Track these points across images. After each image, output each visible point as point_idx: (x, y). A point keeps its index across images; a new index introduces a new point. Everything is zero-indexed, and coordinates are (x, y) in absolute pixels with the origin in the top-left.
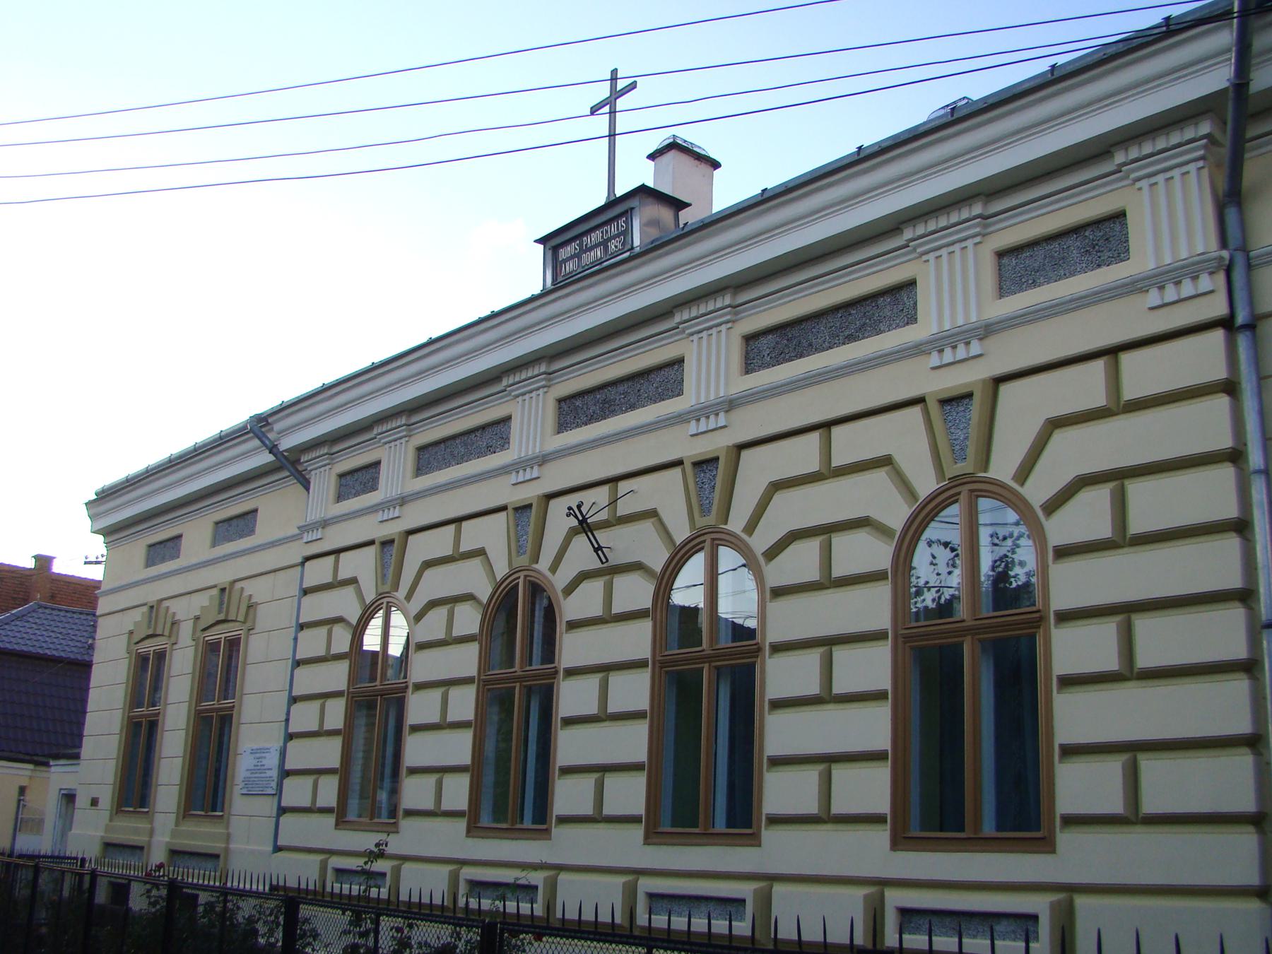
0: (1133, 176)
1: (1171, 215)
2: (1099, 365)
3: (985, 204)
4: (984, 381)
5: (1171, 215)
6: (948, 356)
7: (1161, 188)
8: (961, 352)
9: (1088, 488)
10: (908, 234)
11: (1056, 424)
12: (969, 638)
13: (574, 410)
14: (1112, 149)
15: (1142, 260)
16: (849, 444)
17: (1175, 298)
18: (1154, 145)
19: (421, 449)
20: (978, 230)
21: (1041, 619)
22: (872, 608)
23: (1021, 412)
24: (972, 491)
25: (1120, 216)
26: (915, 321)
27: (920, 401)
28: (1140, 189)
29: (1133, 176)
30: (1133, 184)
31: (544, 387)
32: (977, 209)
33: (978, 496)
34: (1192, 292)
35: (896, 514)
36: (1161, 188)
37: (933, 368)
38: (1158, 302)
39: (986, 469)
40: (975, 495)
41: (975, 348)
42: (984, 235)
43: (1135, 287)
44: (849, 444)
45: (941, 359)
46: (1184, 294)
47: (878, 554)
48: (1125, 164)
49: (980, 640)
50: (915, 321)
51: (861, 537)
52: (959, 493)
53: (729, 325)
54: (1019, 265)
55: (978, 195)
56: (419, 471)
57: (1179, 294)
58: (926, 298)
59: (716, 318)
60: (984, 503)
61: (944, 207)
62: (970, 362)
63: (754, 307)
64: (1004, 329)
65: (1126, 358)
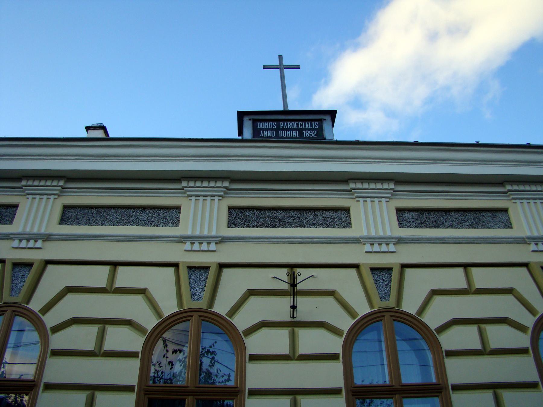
0: (356, 195)
1: (44, 212)
2: (107, 268)
3: (395, 185)
4: (41, 260)
5: (44, 212)
6: (24, 244)
7: (37, 200)
8: (204, 246)
9: (264, 328)
10: (352, 185)
11: (252, 293)
12: (191, 397)
13: (238, 216)
14: (349, 181)
15: (186, 228)
16: (126, 277)
17: (190, 249)
18: (39, 183)
19: (66, 208)
20: (57, 192)
21: (35, 386)
22: (128, 372)
23: (234, 284)
24: (14, 311)
25: (178, 208)
26: (400, 227)
27: (176, 265)
28: (28, 198)
29: (356, 195)
30: (188, 197)
31: (219, 196)
32: (226, 184)
33: (16, 315)
34: (206, 248)
35: (150, 322)
36: (37, 200)
37: (186, 251)
38: (16, 245)
39: (28, 303)
40: (16, 314)
41: (213, 246)
42: (59, 196)
43: (10, 237)
44: (126, 277)
45: (27, 244)
46: (194, 248)
47: (136, 343)
48: (186, 187)
49: (196, 399)
50: (400, 227)
51: (125, 330)
52: (6, 311)
53: (56, 197)
54: (238, 216)
55: (229, 178)
56: (63, 221)
57: (34, 245)
58: (21, 215)
59: (33, 190)
60: (19, 320)
61: (208, 178)
62: (34, 250)
63: (404, 195)
64: (231, 242)
65: (120, 269)
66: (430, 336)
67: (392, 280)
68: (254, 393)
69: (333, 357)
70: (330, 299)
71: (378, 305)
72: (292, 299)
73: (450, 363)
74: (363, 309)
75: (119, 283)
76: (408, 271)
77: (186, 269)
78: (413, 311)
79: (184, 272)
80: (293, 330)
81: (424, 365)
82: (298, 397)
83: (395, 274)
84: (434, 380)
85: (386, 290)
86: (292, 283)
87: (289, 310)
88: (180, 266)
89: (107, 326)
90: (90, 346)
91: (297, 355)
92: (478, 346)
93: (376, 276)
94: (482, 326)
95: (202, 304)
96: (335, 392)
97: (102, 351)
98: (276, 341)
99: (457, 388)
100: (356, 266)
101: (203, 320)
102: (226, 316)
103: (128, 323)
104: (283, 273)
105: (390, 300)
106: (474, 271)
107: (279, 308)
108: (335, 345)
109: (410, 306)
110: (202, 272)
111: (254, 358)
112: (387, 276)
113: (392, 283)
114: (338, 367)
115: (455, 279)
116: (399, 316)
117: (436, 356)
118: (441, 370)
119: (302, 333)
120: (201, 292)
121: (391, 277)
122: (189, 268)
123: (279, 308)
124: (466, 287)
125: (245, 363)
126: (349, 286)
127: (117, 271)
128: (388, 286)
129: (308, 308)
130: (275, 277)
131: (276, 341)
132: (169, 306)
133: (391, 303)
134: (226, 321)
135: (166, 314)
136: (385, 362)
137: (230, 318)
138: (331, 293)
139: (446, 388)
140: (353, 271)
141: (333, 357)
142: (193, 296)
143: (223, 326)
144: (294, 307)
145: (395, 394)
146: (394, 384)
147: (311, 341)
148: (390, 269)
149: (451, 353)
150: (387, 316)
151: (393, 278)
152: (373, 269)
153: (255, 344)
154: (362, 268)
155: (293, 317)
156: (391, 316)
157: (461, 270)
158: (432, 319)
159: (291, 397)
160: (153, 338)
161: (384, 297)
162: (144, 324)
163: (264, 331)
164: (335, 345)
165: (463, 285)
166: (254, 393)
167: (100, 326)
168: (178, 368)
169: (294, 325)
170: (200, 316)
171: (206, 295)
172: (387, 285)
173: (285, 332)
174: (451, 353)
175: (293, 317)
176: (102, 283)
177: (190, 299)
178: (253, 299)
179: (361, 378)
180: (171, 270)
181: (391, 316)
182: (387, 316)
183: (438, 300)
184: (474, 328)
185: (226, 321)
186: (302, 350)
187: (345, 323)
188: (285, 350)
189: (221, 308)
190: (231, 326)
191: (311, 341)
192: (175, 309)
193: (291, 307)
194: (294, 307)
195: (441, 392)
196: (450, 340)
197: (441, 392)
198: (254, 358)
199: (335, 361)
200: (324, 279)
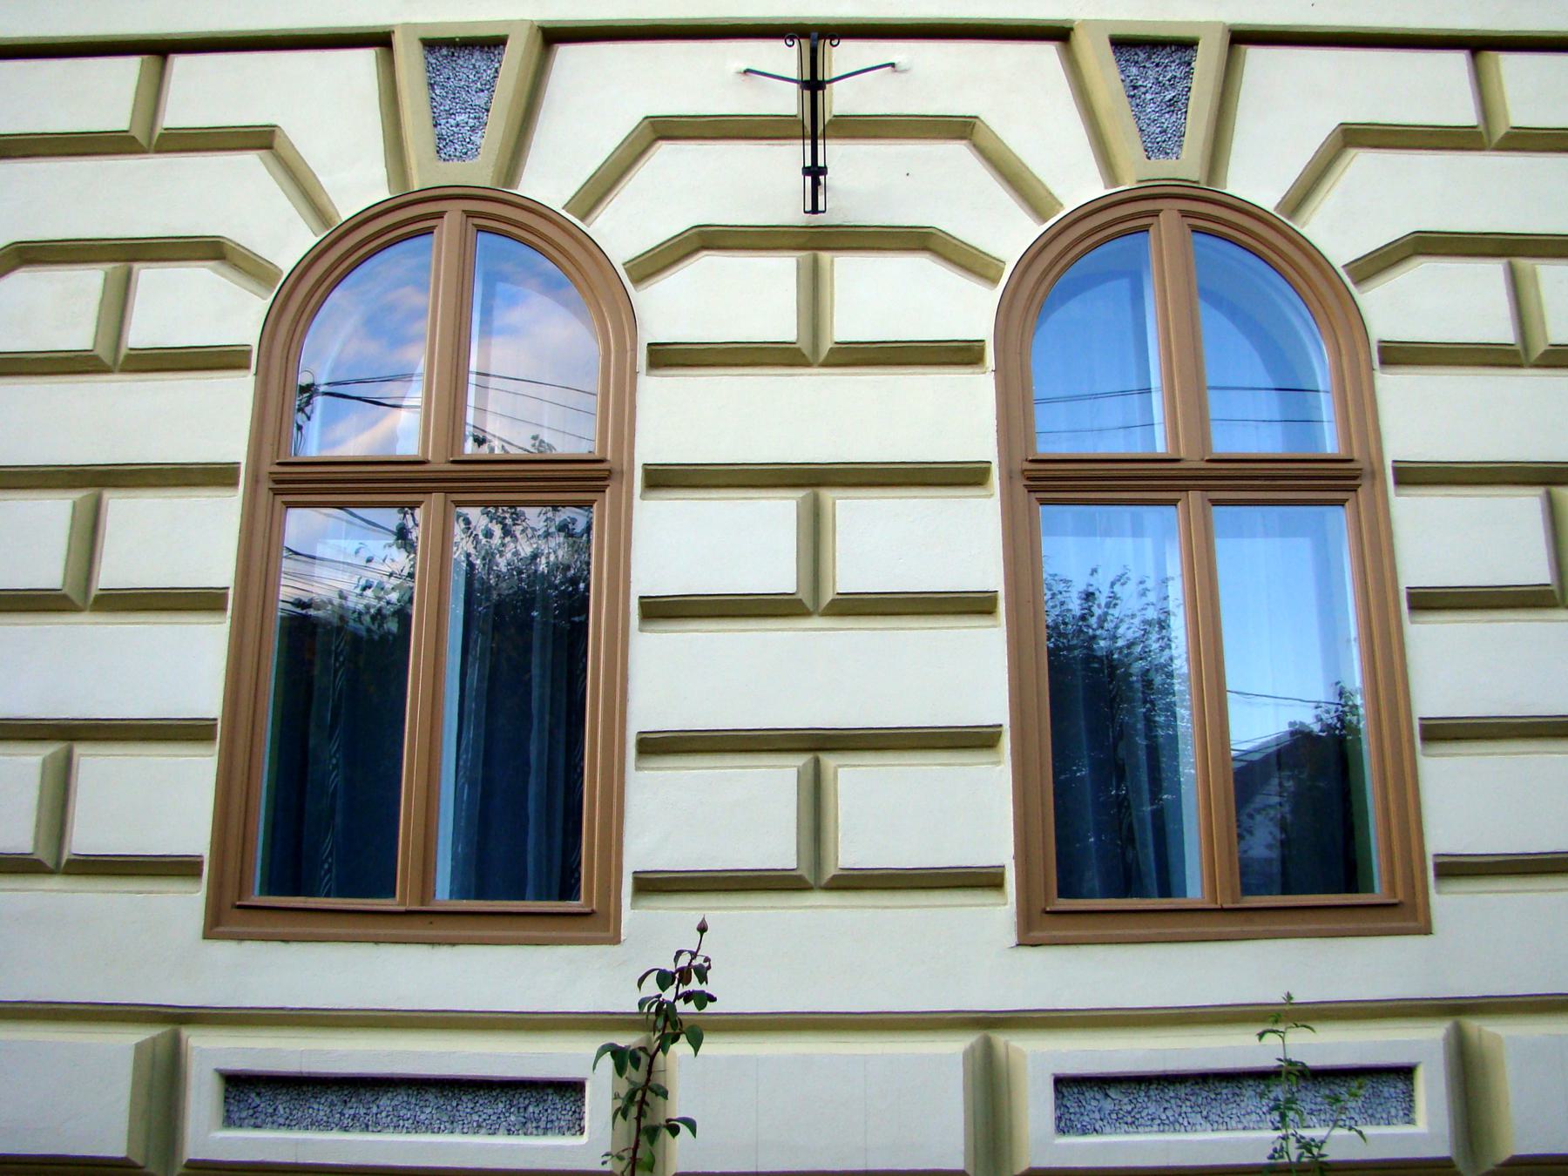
11: (664, 129)
23: (592, 102)
27: (380, 40)
35: (288, 241)
44: (201, 92)
47: (239, 316)
51: (200, 276)
66: (1325, 290)
67: (1194, 86)
68: (662, 479)
69: (963, 354)
70: (958, 151)
71: (1136, 170)
72: (808, 148)
73: (1397, 391)
74: (1078, 184)
75: (178, 114)
76: (1255, 57)
77: (417, 51)
78: (1267, 198)
79: (409, 58)
80: (816, 261)
81: (1293, 389)
82: (828, 495)
83: (1207, 61)
84: (1331, 445)
85: (1168, 120)
86: (807, 77)
87: (798, 183)
88: (397, 40)
89: (136, 266)
90: (80, 337)
91: (826, 346)
92: (1501, 331)
93: (1134, 70)
94: (1523, 263)
95: (478, 172)
96: (967, 476)
97: (124, 351)
98: (750, 297)
99: (1413, 476)
100: (1059, 34)
101: (481, 229)
102: (563, 213)
103: (211, 250)
104: (784, 57)
105: (1183, 156)
106: (1509, 64)
107: (764, 183)
108: (969, 310)
109: (1257, 179)
110: (477, 58)
111: (666, 357)
112: (1174, 70)
113: (1192, 94)
114: (975, 393)
115: (1436, 89)
116: (1216, 218)
117: (1345, 359)
118: (1361, 411)
119: (850, 274)
120: (473, 129)
121: (1188, 75)
122: (431, 45)
123: (764, 183)
124: (1473, 122)
125: (635, 374)
126: (1029, 104)
127: (167, 72)
128: (1175, 106)
129: (865, 180)
130: (747, 71)
131: (750, 297)
132: (357, 183)
133: (1187, 164)
134: (564, 230)
135: (346, 209)
136: (1155, 381)
137: (582, 219)
138: (960, 128)
139: (1375, 474)
140: (1048, 52)
141: (963, 354)
142: (443, 146)
143: (552, 244)
144: (815, 172)
145: (1186, 489)
146: (1182, 455)
147: (877, 296)
148: (1185, 46)
149: (1398, 355)
150: (1169, 212)
151: (1195, 76)
152: (1123, 45)
153: (673, 308)
154: (1081, 40)
155: (815, 210)
156: (1185, 214)
157: (1458, 60)
158: (1339, 229)
159: (800, 493)
160: (301, 296)
161: (1160, 144)
162: (264, 250)
163: (707, 262)
164: (969, 310)
165: (1464, 114)
166: (662, 479)
167: (109, 266)
168: (560, 553)
169: (817, 240)
170: (470, 214)
171: (493, 137)
172: (1172, 103)
173: (783, 268)
174: (1398, 355)
175: (815, 210)
176: (116, 116)
177: (432, 150)
178: (665, 151)
179: (1060, 437)
180: (366, 58)
181: (1185, 214)
182: (1169, 212)
183: (1361, 163)
184: (1494, 270)
185: (564, 230)
186: (846, 326)
187: (1010, 234)
188: (783, 327)
189: (548, 181)
190: (572, 236)
191: (877, 296)
192: (380, 192)
193: (806, 171)
194: (815, 172)
195: (1354, 489)
196: (1398, 307)
197: (1354, 489)
198: (666, 357)
199: (969, 370)
200: (935, 78)
